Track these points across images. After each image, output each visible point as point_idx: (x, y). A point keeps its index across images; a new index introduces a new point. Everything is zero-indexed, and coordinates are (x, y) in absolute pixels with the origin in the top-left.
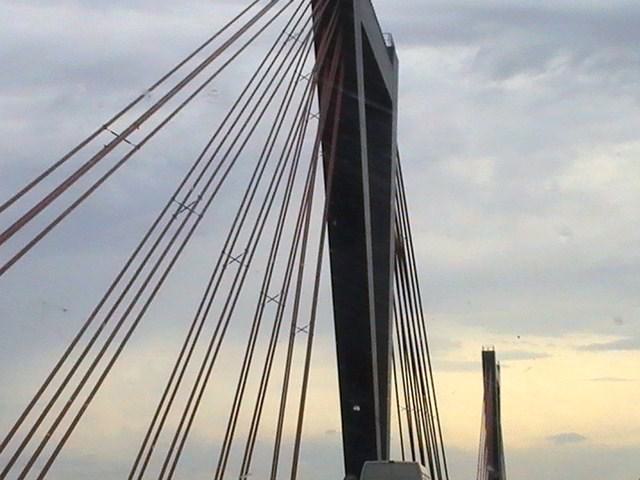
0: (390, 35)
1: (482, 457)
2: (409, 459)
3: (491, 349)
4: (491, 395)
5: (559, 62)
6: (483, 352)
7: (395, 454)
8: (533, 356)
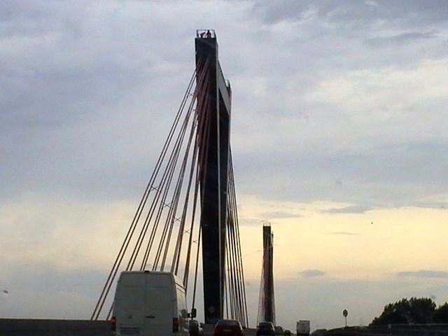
0: (228, 81)
1: (262, 290)
2: (230, 318)
3: (269, 225)
4: (267, 255)
5: (310, 14)
6: (264, 227)
7: (225, 318)
8: (290, 216)
